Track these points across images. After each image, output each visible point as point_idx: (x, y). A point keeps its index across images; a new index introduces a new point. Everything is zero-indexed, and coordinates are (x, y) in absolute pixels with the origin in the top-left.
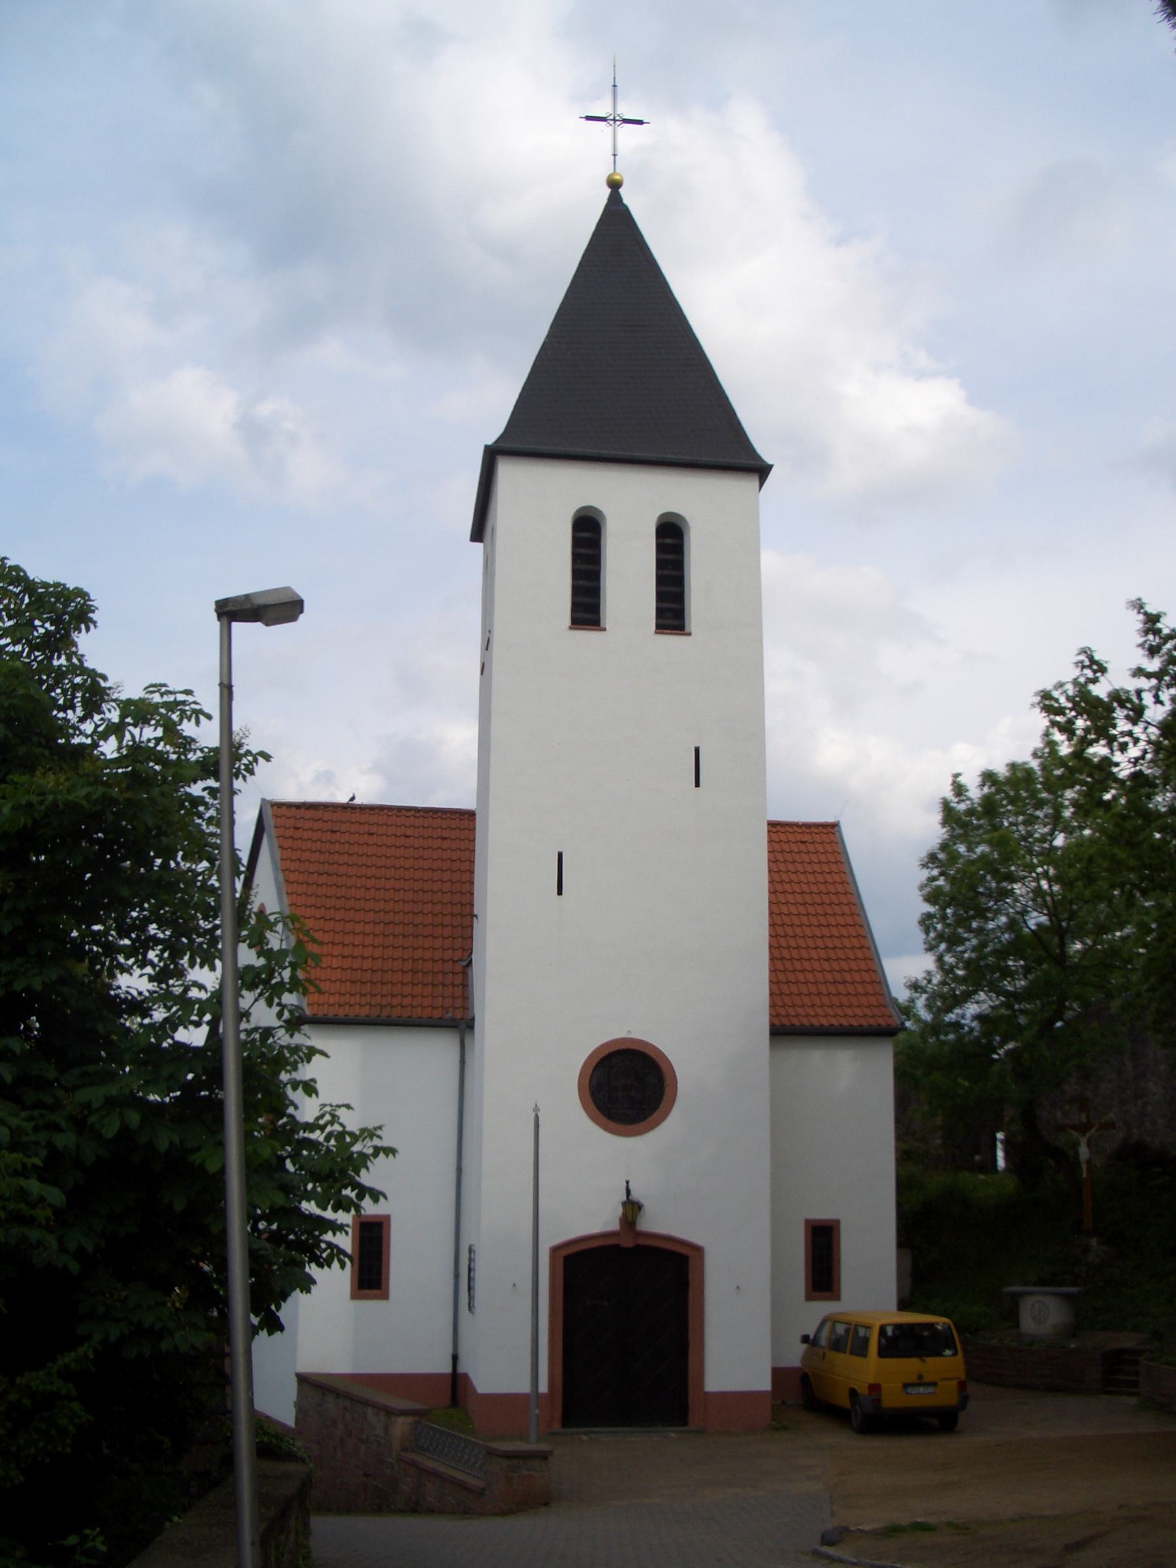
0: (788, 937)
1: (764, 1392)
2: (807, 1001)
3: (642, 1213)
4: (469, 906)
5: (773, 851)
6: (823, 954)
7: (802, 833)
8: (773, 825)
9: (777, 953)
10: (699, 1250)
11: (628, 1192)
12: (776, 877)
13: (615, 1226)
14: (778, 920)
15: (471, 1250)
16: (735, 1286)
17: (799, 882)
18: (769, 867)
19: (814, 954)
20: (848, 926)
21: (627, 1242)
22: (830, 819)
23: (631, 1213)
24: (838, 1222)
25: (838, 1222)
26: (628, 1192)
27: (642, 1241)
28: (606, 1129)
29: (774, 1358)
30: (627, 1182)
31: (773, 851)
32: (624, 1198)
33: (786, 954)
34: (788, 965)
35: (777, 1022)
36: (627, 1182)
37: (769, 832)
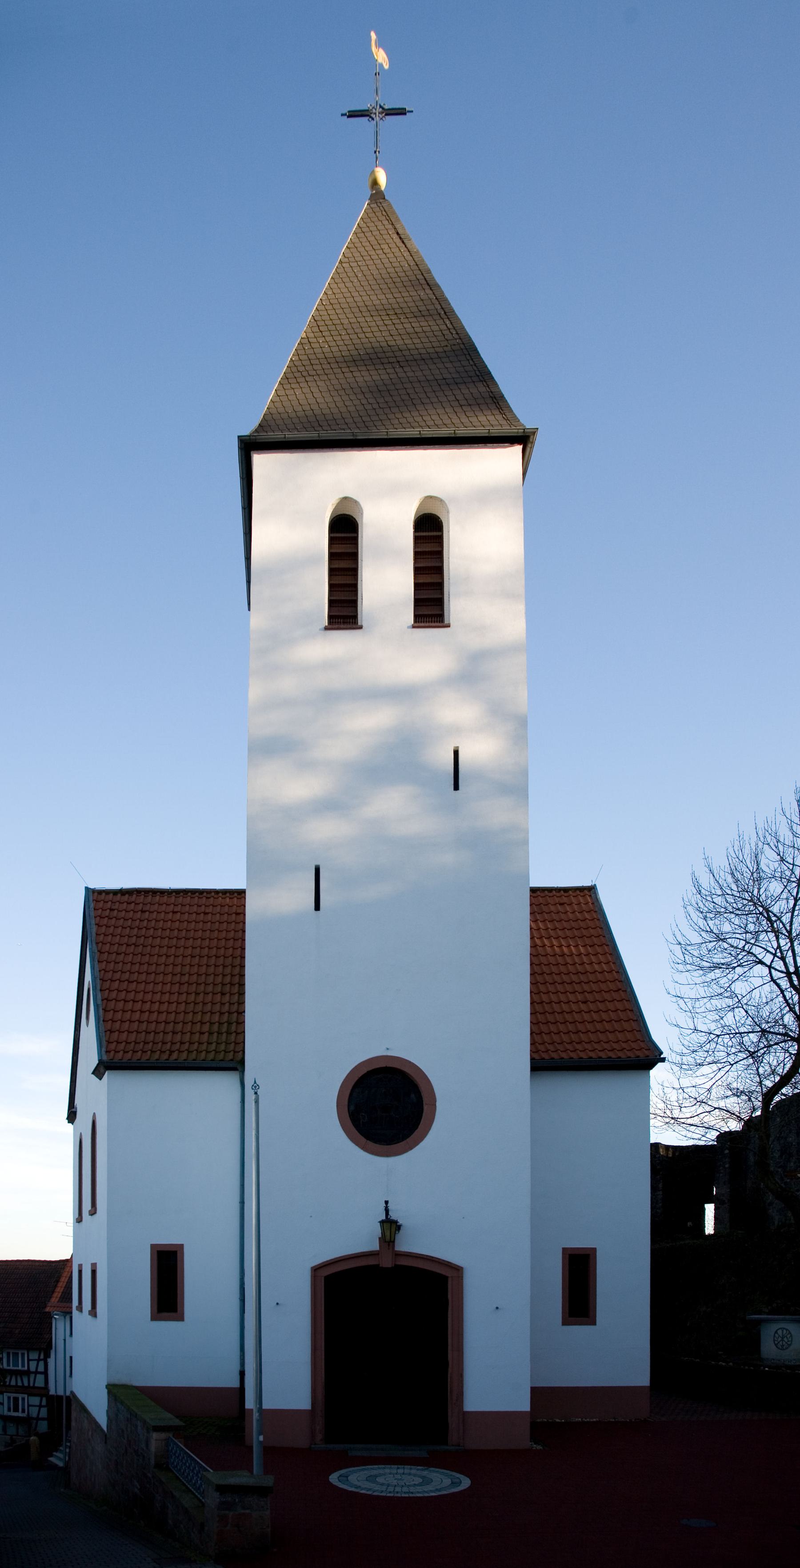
0: (543, 1034)
1: (525, 1412)
2: (565, 1038)
3: (401, 1232)
4: (241, 924)
5: (538, 1023)
6: (580, 997)
7: (560, 897)
8: (533, 890)
9: (536, 998)
10: (458, 1270)
11: (387, 1211)
12: (538, 1008)
13: (375, 1246)
14: (539, 978)
15: (71, 1358)
16: (495, 1306)
17: (551, 974)
18: (531, 926)
19: (571, 997)
20: (600, 983)
21: (387, 1262)
22: (587, 883)
23: (389, 1232)
24: (594, 1250)
25: (594, 1250)
26: (387, 1211)
27: (403, 1262)
28: (364, 1148)
29: (535, 1358)
30: (387, 1202)
31: (538, 1023)
32: (384, 1218)
33: (545, 998)
34: (547, 1008)
35: (536, 1056)
36: (387, 1202)
37: (531, 896)
